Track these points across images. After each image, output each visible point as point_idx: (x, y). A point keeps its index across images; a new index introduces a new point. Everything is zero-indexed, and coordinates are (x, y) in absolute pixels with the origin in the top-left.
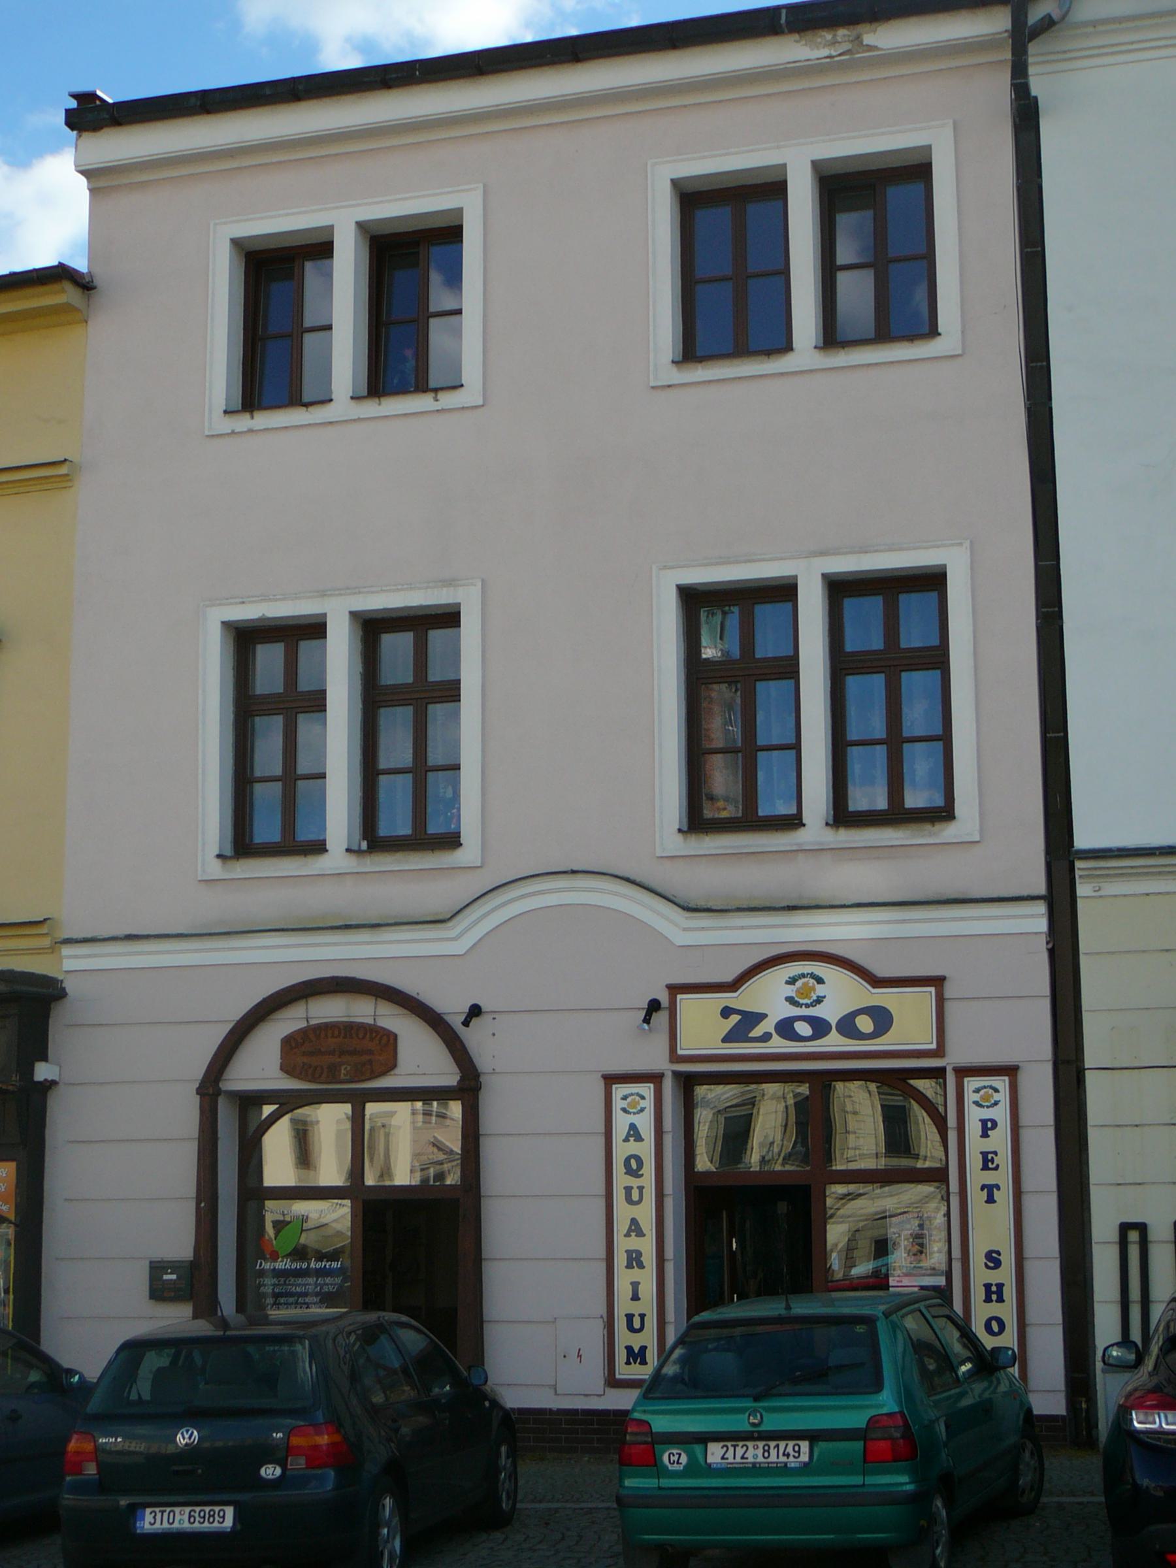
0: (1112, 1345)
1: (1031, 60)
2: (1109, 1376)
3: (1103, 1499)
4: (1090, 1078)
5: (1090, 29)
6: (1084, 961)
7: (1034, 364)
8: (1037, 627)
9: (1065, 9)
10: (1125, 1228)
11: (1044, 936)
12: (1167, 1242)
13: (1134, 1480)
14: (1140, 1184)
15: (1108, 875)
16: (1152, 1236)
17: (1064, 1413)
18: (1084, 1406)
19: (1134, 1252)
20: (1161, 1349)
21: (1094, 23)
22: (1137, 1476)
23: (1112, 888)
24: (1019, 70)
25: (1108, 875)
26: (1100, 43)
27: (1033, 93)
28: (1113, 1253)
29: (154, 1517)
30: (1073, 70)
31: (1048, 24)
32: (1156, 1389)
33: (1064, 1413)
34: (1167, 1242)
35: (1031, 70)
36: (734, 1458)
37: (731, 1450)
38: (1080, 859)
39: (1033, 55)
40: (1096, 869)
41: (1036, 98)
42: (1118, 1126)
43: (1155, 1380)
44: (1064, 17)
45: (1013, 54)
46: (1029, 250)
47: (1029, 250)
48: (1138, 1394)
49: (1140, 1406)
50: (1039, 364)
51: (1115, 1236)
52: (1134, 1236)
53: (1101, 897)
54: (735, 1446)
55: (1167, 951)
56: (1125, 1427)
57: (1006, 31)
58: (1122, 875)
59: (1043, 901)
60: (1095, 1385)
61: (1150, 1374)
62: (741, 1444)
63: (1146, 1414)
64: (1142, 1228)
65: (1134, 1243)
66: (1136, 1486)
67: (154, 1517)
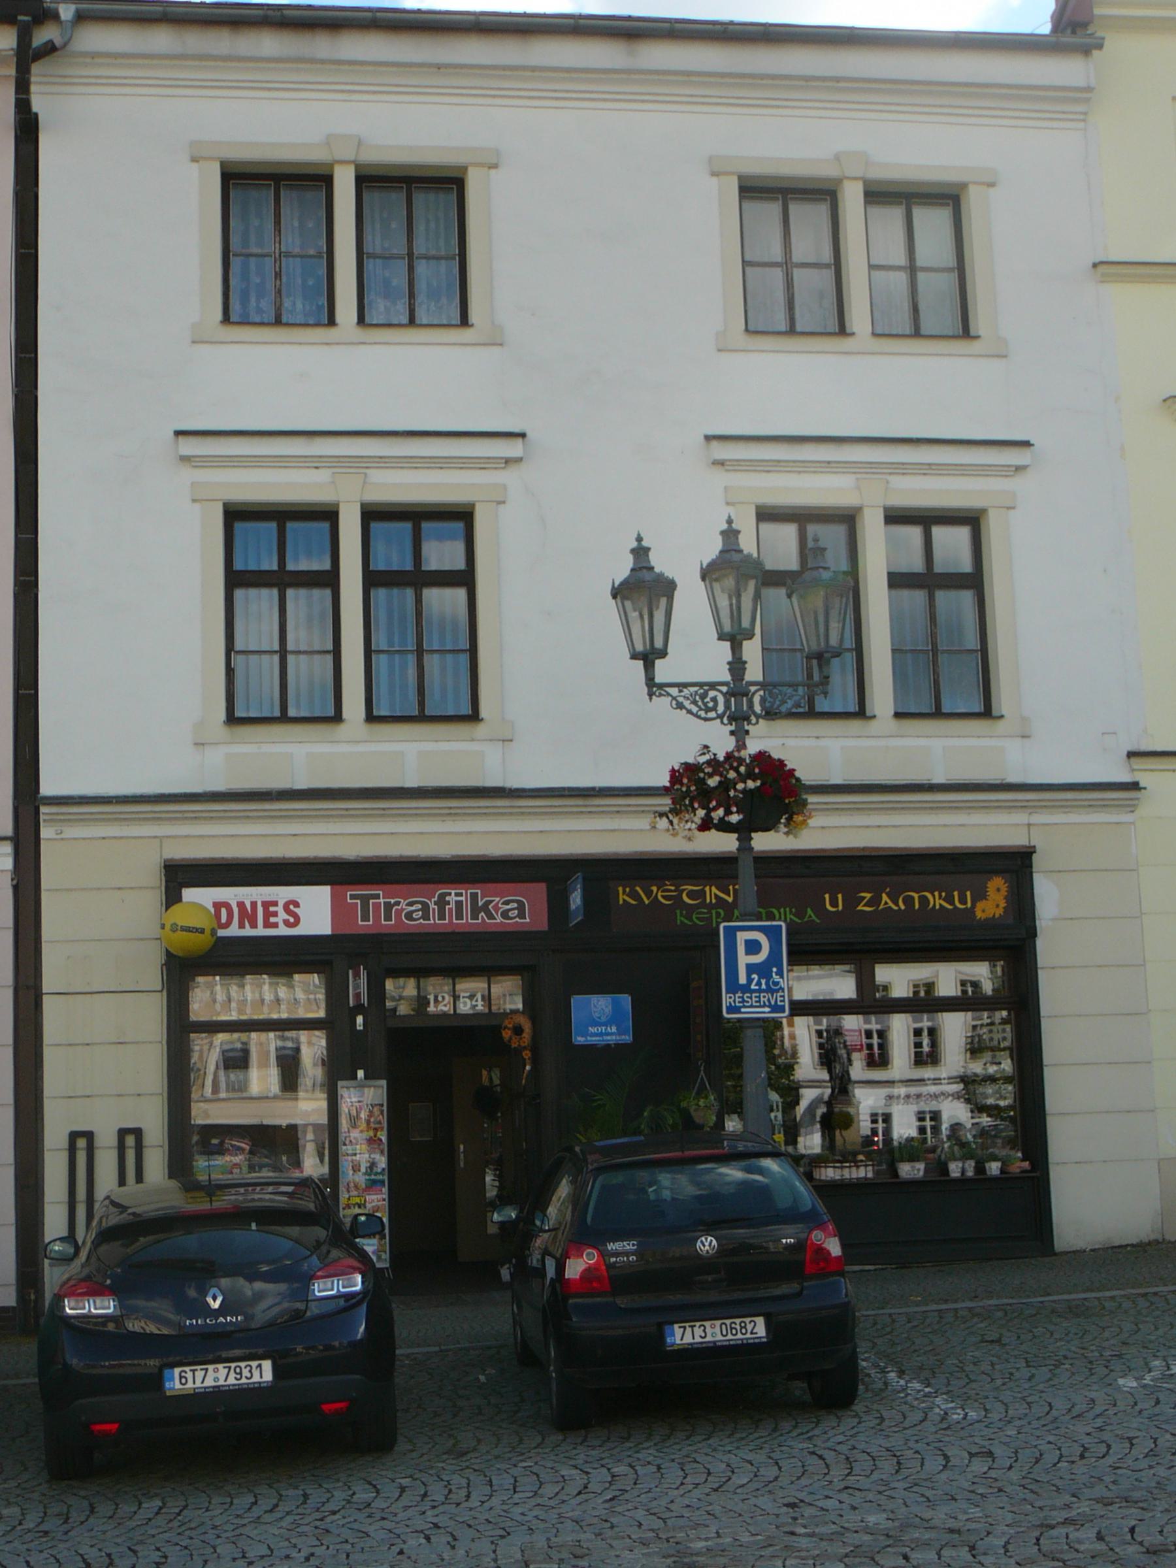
0: (55, 1240)
1: (33, 79)
2: (55, 1269)
3: (37, 1380)
4: (48, 1003)
5: (88, 60)
6: (45, 897)
7: (23, 355)
8: (15, 594)
9: (66, 39)
10: (74, 1136)
11: (10, 874)
12: (110, 1148)
13: (64, 1360)
14: (88, 1096)
15: (69, 820)
16: (99, 1141)
17: (14, 1304)
18: (33, 1297)
19: (81, 1158)
20: (93, 1242)
21: (94, 55)
22: (68, 1357)
23: (71, 832)
24: (23, 86)
25: (69, 820)
26: (99, 74)
27: (35, 109)
28: (64, 1157)
29: (704, 1331)
30: (66, 94)
31: (50, 49)
32: (88, 1278)
33: (14, 1304)
34: (110, 1148)
35: (33, 88)
36: (194, 1383)
37: (689, 1330)
38: (45, 804)
39: (36, 75)
40: (57, 814)
41: (36, 115)
42: (70, 1045)
43: (86, 1271)
44: (65, 45)
45: (17, 71)
46: (23, 251)
47: (23, 251)
48: (72, 1282)
49: (72, 1294)
50: (27, 356)
51: (64, 1142)
52: (82, 1143)
53: (62, 839)
54: (692, 1327)
55: (119, 889)
56: (59, 1314)
57: (12, 49)
58: (82, 820)
59: (9, 842)
60: (43, 1278)
61: (83, 1266)
62: (698, 1324)
63: (77, 1301)
64: (89, 1136)
65: (82, 1149)
66: (65, 1365)
67: (704, 1331)
